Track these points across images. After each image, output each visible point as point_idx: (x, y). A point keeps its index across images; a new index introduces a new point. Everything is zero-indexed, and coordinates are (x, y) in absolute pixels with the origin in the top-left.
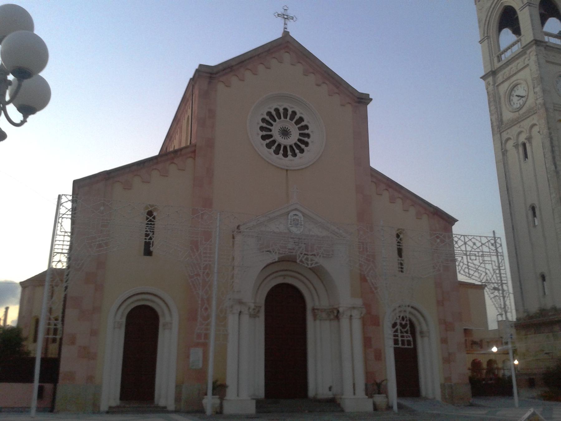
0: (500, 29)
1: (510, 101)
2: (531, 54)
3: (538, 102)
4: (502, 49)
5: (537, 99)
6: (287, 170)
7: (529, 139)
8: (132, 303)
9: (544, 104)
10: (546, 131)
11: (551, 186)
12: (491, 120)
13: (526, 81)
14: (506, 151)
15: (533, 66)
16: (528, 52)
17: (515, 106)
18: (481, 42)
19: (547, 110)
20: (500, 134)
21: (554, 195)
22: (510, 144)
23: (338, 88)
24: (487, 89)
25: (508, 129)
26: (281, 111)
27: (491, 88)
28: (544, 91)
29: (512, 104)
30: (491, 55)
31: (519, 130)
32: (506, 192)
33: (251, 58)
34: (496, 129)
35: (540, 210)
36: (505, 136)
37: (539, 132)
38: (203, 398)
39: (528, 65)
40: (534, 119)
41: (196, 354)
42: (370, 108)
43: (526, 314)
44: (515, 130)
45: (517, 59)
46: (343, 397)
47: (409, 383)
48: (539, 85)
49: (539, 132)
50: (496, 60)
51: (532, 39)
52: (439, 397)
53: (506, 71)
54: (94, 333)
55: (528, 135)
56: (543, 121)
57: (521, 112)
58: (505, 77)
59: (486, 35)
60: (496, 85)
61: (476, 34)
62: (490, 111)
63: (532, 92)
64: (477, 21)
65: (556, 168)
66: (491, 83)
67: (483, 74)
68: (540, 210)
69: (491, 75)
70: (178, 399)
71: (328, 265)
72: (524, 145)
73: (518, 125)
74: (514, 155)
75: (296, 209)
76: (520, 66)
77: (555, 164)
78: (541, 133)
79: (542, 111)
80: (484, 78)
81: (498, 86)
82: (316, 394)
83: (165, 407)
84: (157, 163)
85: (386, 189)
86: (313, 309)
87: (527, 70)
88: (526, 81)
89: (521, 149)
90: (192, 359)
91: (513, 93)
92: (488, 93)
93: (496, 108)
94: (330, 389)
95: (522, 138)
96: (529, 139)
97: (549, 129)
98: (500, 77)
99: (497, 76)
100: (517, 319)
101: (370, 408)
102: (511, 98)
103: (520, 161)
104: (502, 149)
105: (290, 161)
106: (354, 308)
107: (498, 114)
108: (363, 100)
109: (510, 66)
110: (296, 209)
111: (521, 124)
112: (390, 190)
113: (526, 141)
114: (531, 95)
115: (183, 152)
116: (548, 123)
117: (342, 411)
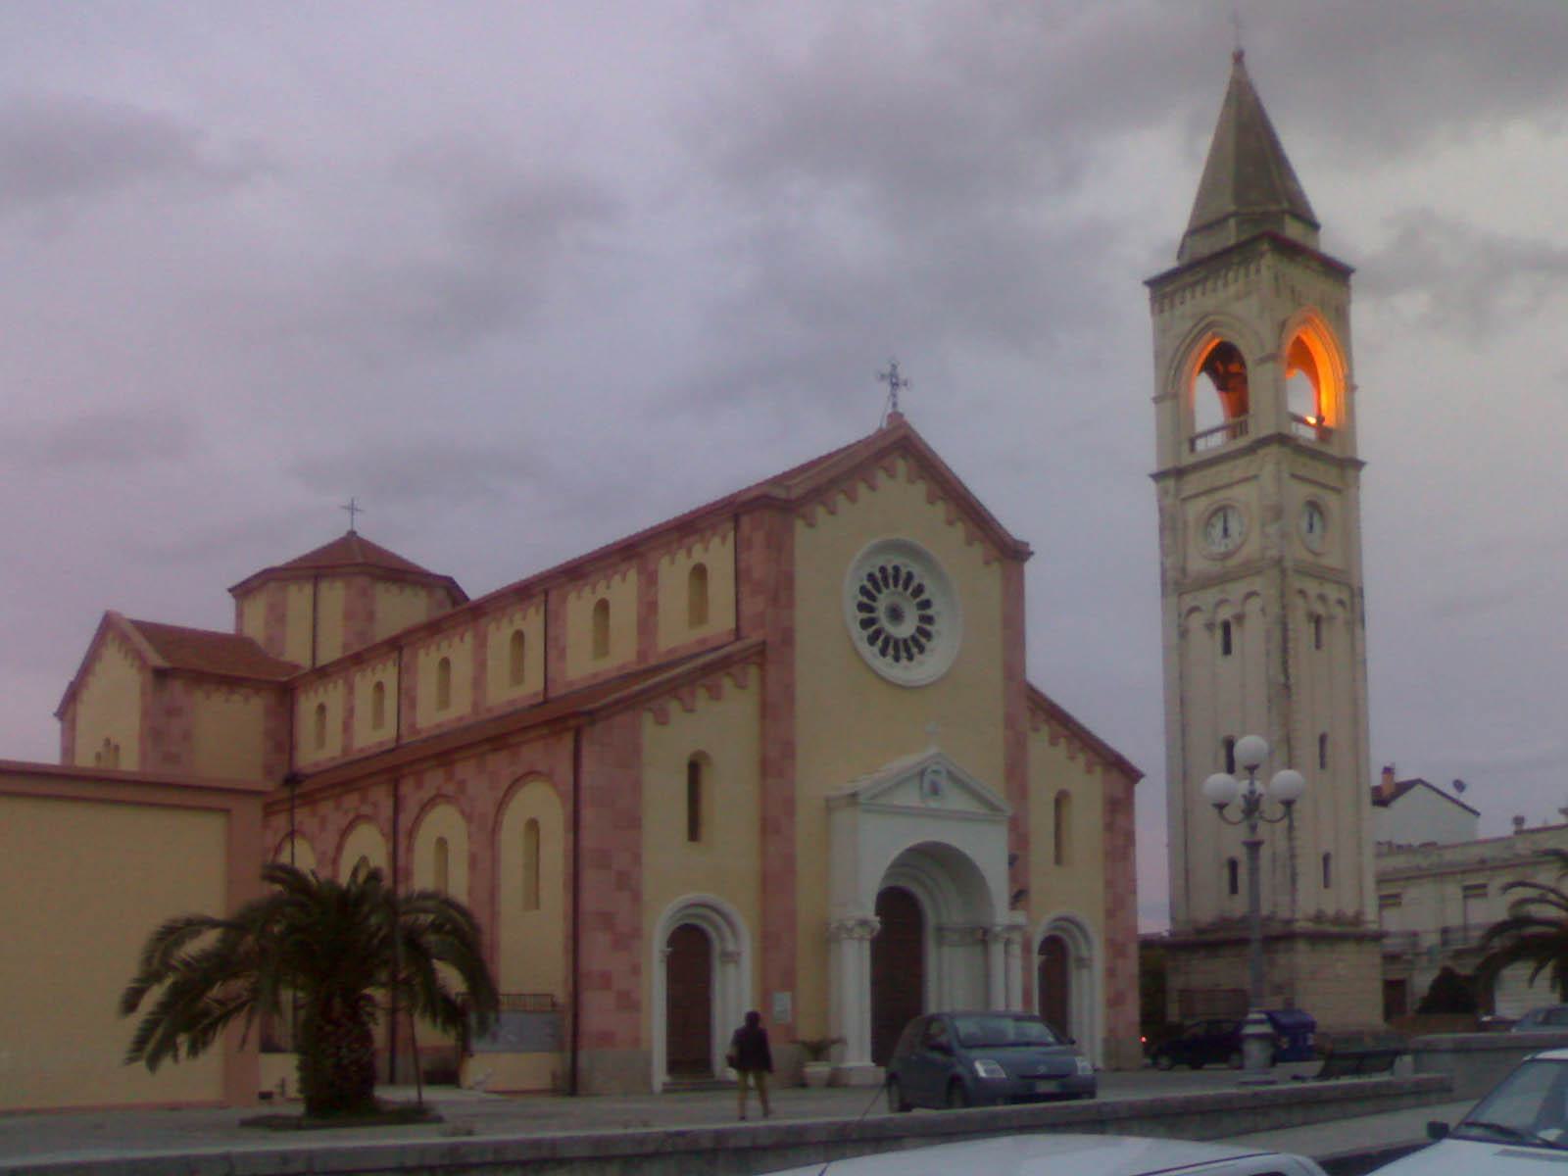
0: (1201, 371)
7: (1240, 618)
10: (1275, 609)
12: (1162, 564)
16: (1261, 452)
22: (1197, 622)
26: (890, 571)
39: (1255, 477)
40: (1257, 583)
42: (1030, 567)
44: (1209, 597)
50: (1186, 447)
54: (636, 970)
62: (1162, 546)
67: (1154, 468)
72: (1227, 627)
80: (1158, 477)
81: (1184, 500)
89: (1219, 633)
95: (1225, 613)
96: (1240, 618)
98: (1193, 483)
105: (885, 666)
111: (1230, 587)
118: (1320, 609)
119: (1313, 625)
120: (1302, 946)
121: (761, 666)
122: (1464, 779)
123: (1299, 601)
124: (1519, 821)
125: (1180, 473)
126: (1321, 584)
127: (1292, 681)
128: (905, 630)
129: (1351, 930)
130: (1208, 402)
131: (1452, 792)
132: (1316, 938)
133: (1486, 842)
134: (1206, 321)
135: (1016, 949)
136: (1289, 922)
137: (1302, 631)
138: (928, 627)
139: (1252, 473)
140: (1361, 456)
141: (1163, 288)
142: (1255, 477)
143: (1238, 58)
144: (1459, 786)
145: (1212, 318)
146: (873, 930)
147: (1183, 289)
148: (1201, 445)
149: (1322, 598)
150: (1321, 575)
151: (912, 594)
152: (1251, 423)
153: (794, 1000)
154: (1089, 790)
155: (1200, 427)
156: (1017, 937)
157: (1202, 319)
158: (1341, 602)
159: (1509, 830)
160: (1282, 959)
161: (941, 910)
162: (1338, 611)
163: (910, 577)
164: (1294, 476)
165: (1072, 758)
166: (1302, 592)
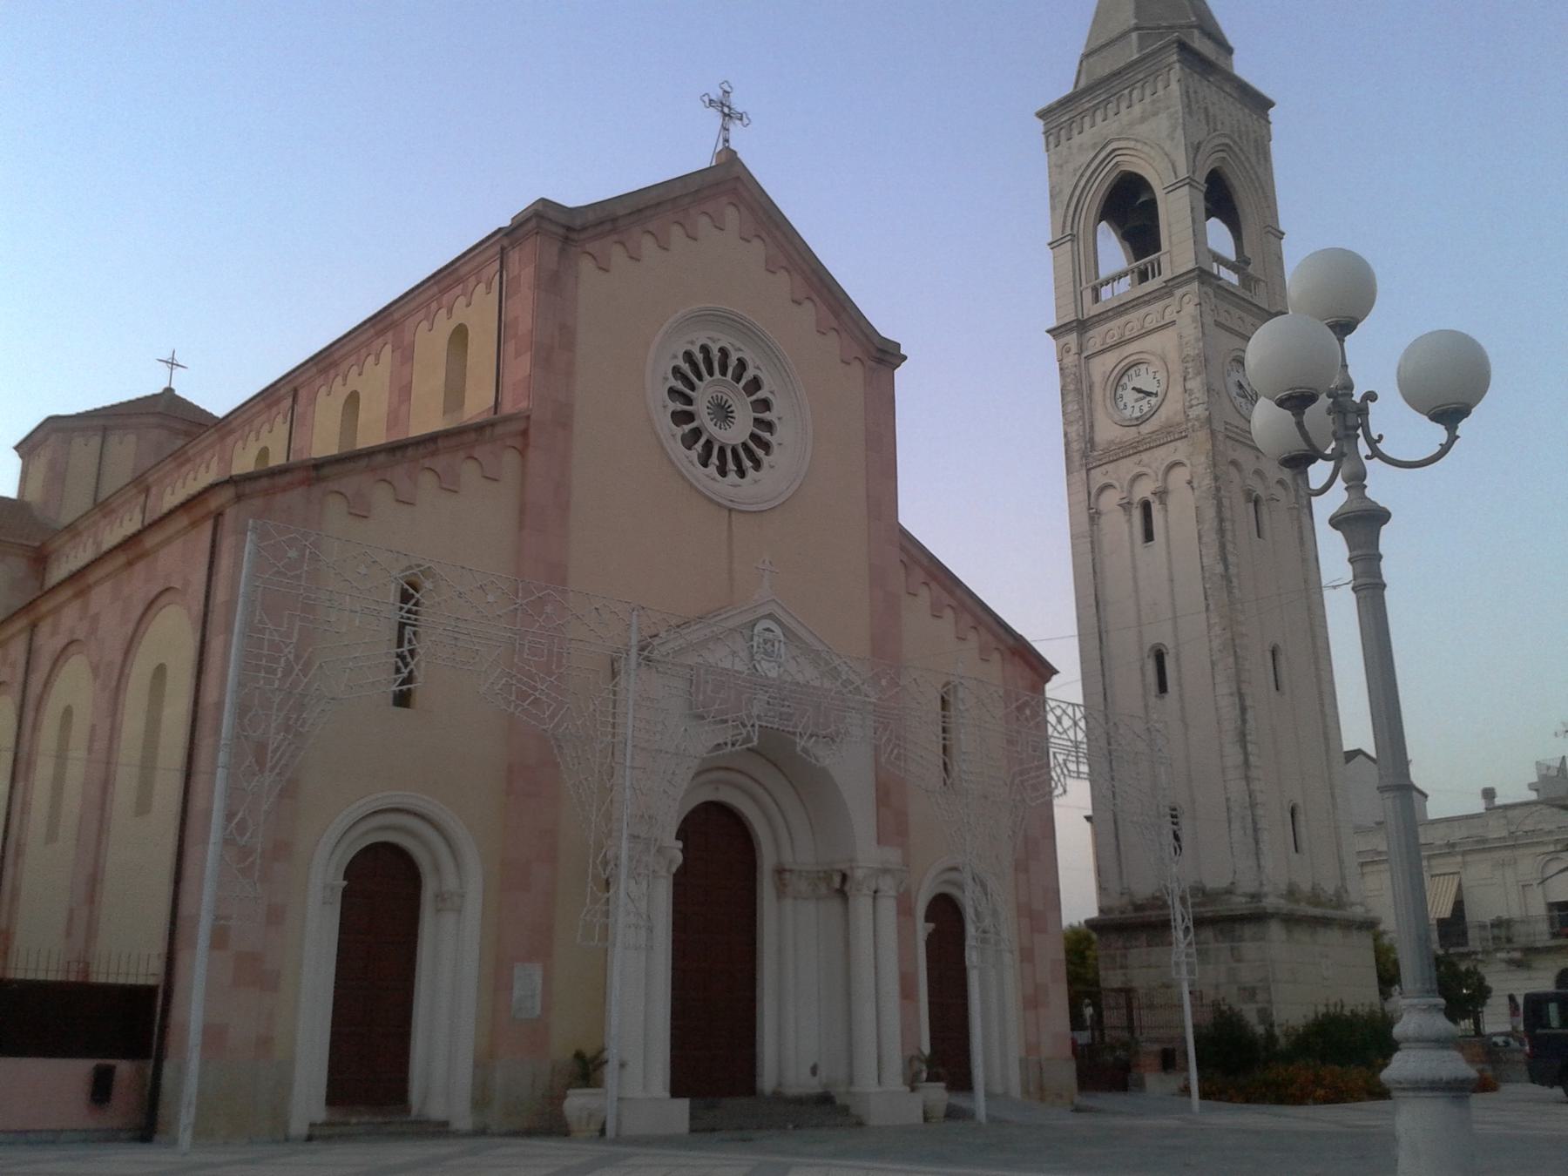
1: (1116, 398)
2: (1186, 299)
3: (1193, 413)
4: (1103, 274)
6: (730, 510)
7: (1162, 494)
8: (366, 833)
9: (1209, 420)
10: (1207, 481)
11: (1212, 607)
12: (1066, 435)
15: (1187, 325)
16: (1179, 292)
17: (1128, 413)
18: (1053, 245)
19: (1213, 433)
20: (1088, 470)
21: (1217, 630)
22: (1110, 500)
23: (837, 316)
24: (1060, 361)
27: (1070, 359)
28: (1209, 390)
30: (1077, 281)
31: (1139, 469)
32: (1094, 610)
33: (659, 204)
34: (1076, 457)
36: (1099, 477)
37: (1189, 482)
38: (565, 1097)
40: (1179, 451)
41: (527, 981)
42: (902, 376)
43: (1125, 900)
44: (1128, 467)
45: (1147, 303)
46: (854, 1089)
47: (948, 1057)
48: (1199, 373)
49: (1189, 482)
50: (1088, 295)
51: (1191, 266)
52: (1016, 1091)
53: (1114, 327)
54: (275, 916)
56: (1202, 460)
57: (1146, 429)
58: (1110, 341)
59: (1068, 231)
61: (1042, 225)
63: (1180, 389)
64: (1048, 195)
65: (1226, 568)
66: (1074, 349)
67: (1053, 324)
69: (1073, 329)
70: (480, 1101)
71: (826, 758)
72: (1146, 507)
73: (1136, 458)
74: (1120, 528)
75: (770, 616)
76: (1151, 323)
77: (1224, 560)
78: (1195, 485)
79: (1202, 435)
82: (780, 1085)
83: (446, 1124)
84: (434, 454)
85: (926, 584)
86: (780, 871)
87: (1170, 333)
89: (1137, 514)
90: (517, 993)
91: (1125, 380)
93: (1082, 409)
94: (814, 1071)
95: (1144, 490)
96: (1162, 494)
97: (1216, 478)
99: (1090, 334)
100: (1101, 910)
101: (917, 1117)
102: (1120, 391)
105: (727, 487)
106: (886, 871)
109: (1126, 318)
110: (770, 616)
111: (1145, 456)
112: (933, 585)
113: (1151, 498)
114: (1176, 391)
115: (499, 430)
116: (1215, 465)
117: (860, 1124)
118: (1260, 491)
119: (1251, 505)
120: (1275, 930)
121: (522, 453)
124: (1489, 794)
125: (1081, 326)
127: (1233, 570)
128: (737, 433)
129: (1330, 913)
130: (1111, 251)
132: (1291, 921)
135: (888, 907)
136: (1256, 897)
137: (1245, 511)
138: (766, 416)
141: (1059, 118)
145: (1114, 145)
146: (671, 862)
147: (1082, 115)
148: (1106, 293)
149: (1258, 472)
151: (744, 388)
152: (1165, 261)
153: (547, 980)
155: (1104, 273)
156: (888, 885)
158: (1281, 482)
159: (1479, 806)
160: (1249, 948)
161: (782, 842)
162: (1279, 492)
163: (742, 364)
164: (1217, 324)
166: (1234, 463)
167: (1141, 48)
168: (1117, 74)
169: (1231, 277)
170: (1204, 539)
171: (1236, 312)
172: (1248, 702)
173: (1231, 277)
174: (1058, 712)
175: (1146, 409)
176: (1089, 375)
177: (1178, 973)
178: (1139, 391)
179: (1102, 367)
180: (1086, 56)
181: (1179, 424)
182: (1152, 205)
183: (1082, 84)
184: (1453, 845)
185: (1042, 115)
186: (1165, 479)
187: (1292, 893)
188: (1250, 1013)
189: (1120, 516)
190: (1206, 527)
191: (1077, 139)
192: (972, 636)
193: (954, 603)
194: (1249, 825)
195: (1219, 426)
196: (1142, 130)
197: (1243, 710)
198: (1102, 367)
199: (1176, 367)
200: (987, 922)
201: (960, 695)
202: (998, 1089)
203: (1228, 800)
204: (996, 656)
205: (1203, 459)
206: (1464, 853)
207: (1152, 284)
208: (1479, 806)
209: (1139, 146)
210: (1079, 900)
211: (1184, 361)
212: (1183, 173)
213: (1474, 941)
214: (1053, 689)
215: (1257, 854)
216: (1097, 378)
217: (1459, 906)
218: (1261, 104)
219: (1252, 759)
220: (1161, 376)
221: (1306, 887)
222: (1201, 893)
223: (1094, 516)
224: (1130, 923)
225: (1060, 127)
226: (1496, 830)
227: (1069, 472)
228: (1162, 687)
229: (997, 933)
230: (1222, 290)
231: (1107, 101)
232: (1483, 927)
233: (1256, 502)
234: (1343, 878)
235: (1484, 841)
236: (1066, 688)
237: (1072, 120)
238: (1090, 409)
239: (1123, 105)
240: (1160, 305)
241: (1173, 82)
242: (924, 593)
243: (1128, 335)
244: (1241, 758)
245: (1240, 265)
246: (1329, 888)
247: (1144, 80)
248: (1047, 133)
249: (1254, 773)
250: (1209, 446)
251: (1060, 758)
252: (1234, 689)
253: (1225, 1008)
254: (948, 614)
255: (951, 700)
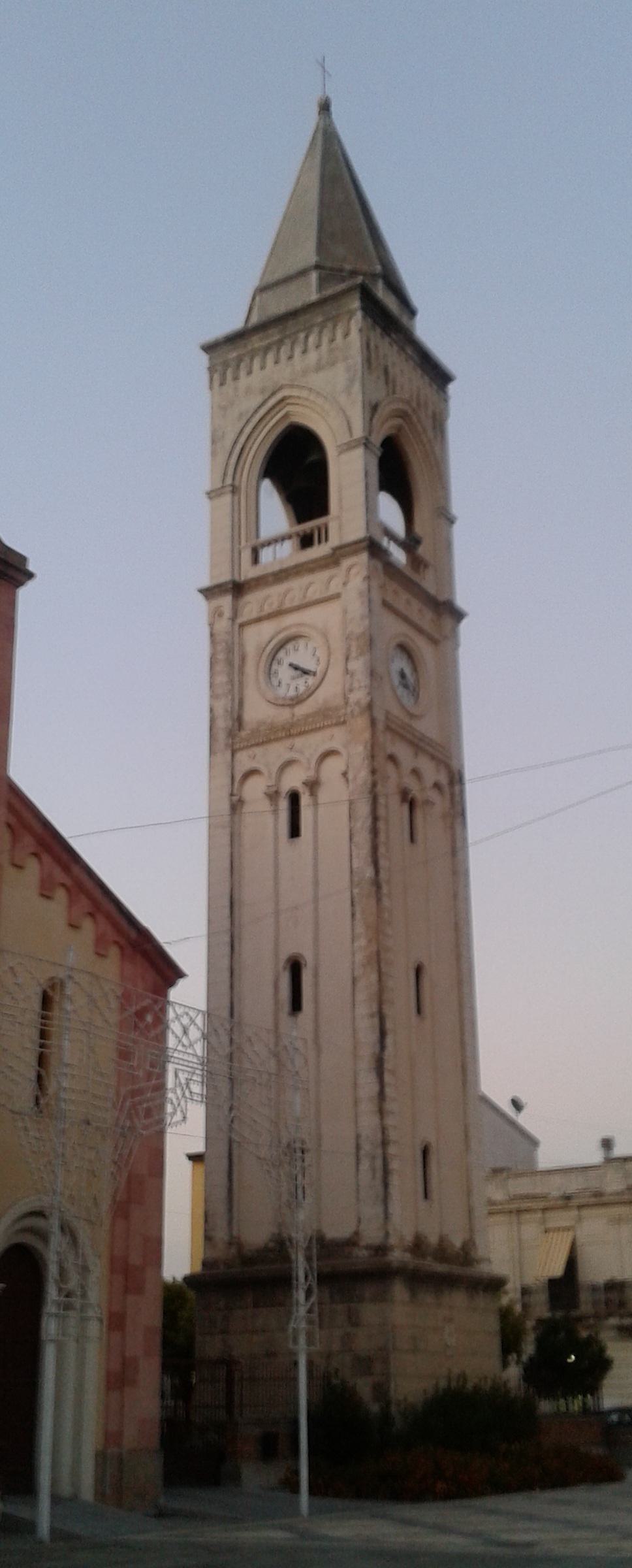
1: (269, 673)
2: (353, 571)
5: (351, 690)
7: (313, 785)
9: (370, 706)
10: (363, 775)
11: (358, 916)
12: (211, 710)
13: (325, 635)
14: (241, 802)
16: (346, 563)
17: (282, 692)
18: (212, 495)
19: (373, 722)
21: (362, 942)
22: (255, 789)
24: (211, 625)
25: (258, 745)
27: (223, 624)
28: (372, 674)
29: (275, 683)
30: (235, 538)
31: (288, 756)
34: (222, 736)
35: (316, 975)
36: (244, 761)
37: (345, 774)
39: (337, 596)
40: (334, 738)
44: (277, 753)
48: (361, 654)
49: (345, 774)
50: (247, 555)
53: (273, 595)
55: (272, 782)
56: (358, 752)
57: (301, 710)
58: (267, 609)
60: (239, 620)
65: (377, 872)
66: (227, 613)
67: (206, 583)
68: (316, 975)
72: (294, 798)
73: (288, 743)
76: (314, 593)
77: (376, 863)
78: (350, 776)
79: (362, 723)
80: (209, 592)
81: (242, 626)
85: (35, 854)
87: (334, 608)
88: (325, 635)
89: (284, 804)
91: (281, 654)
92: (212, 635)
93: (231, 682)
95: (294, 779)
96: (313, 785)
97: (373, 772)
98: (252, 603)
102: (275, 667)
103: (276, 838)
104: (232, 795)
107: (233, 700)
108: (11, 572)
111: (298, 742)
112: (46, 858)
118: (411, 783)
119: (406, 807)
122: (523, 1099)
123: (390, 768)
124: (607, 1144)
125: (238, 589)
126: (416, 754)
127: (383, 875)
129: (456, 1270)
130: (274, 512)
131: (509, 1110)
132: (417, 1279)
133: (549, 1172)
134: (279, 396)
136: (381, 1250)
137: (396, 813)
139: (333, 590)
140: (461, 602)
141: (228, 352)
142: (337, 596)
143: (325, 107)
144: (517, 1105)
148: (266, 555)
149: (415, 772)
150: (418, 744)
154: (94, 981)
155: (266, 533)
157: (273, 394)
158: (437, 786)
159: (596, 1156)
160: (369, 1312)
162: (433, 795)
165: (74, 926)
166: (392, 758)
167: (321, 287)
168: (293, 314)
169: (399, 556)
170: (355, 839)
171: (404, 596)
172: (389, 1025)
173: (399, 556)
174: (185, 1021)
175: (302, 689)
176: (241, 645)
177: (295, 1341)
178: (296, 668)
179: (257, 637)
180: (262, 289)
181: (337, 709)
182: (321, 467)
183: (255, 319)
184: (568, 1198)
185: (209, 348)
186: (318, 770)
187: (418, 1246)
188: (364, 1388)
189: (266, 805)
190: (359, 825)
191: (244, 381)
192: (88, 925)
193: (68, 882)
194: (379, 1163)
195: (380, 716)
196: (317, 380)
197: (383, 1034)
198: (257, 637)
199: (338, 645)
200: (73, 1283)
201: (68, 992)
202: (66, 1490)
203: (358, 1137)
204: (114, 952)
205: (360, 749)
206: (580, 1207)
207: (317, 551)
208: (596, 1156)
209: (312, 397)
210: (179, 1258)
211: (348, 638)
212: (359, 432)
213: (585, 1306)
214: (176, 993)
215: (386, 1199)
216: (251, 648)
217: (572, 1264)
218: (440, 377)
219: (388, 1090)
220: (321, 653)
221: (433, 1240)
222: (324, 1247)
223: (236, 805)
224: (243, 1277)
225: (226, 365)
226: (613, 1183)
227: (212, 752)
228: (296, 1005)
229: (84, 1295)
230: (390, 568)
231: (280, 343)
232: (594, 1288)
233: (412, 805)
234: (471, 1230)
235: (598, 1194)
236: (189, 997)
237: (240, 360)
238: (241, 683)
239: (298, 350)
240: (324, 575)
241: (353, 332)
242: (33, 866)
243: (287, 605)
244: (375, 1088)
245: (411, 543)
246: (457, 1242)
247: (322, 326)
248: (212, 370)
249: (389, 1106)
250: (367, 735)
251: (182, 1077)
252: (375, 1008)
253: (335, 1381)
254: (61, 895)
255: (57, 998)
